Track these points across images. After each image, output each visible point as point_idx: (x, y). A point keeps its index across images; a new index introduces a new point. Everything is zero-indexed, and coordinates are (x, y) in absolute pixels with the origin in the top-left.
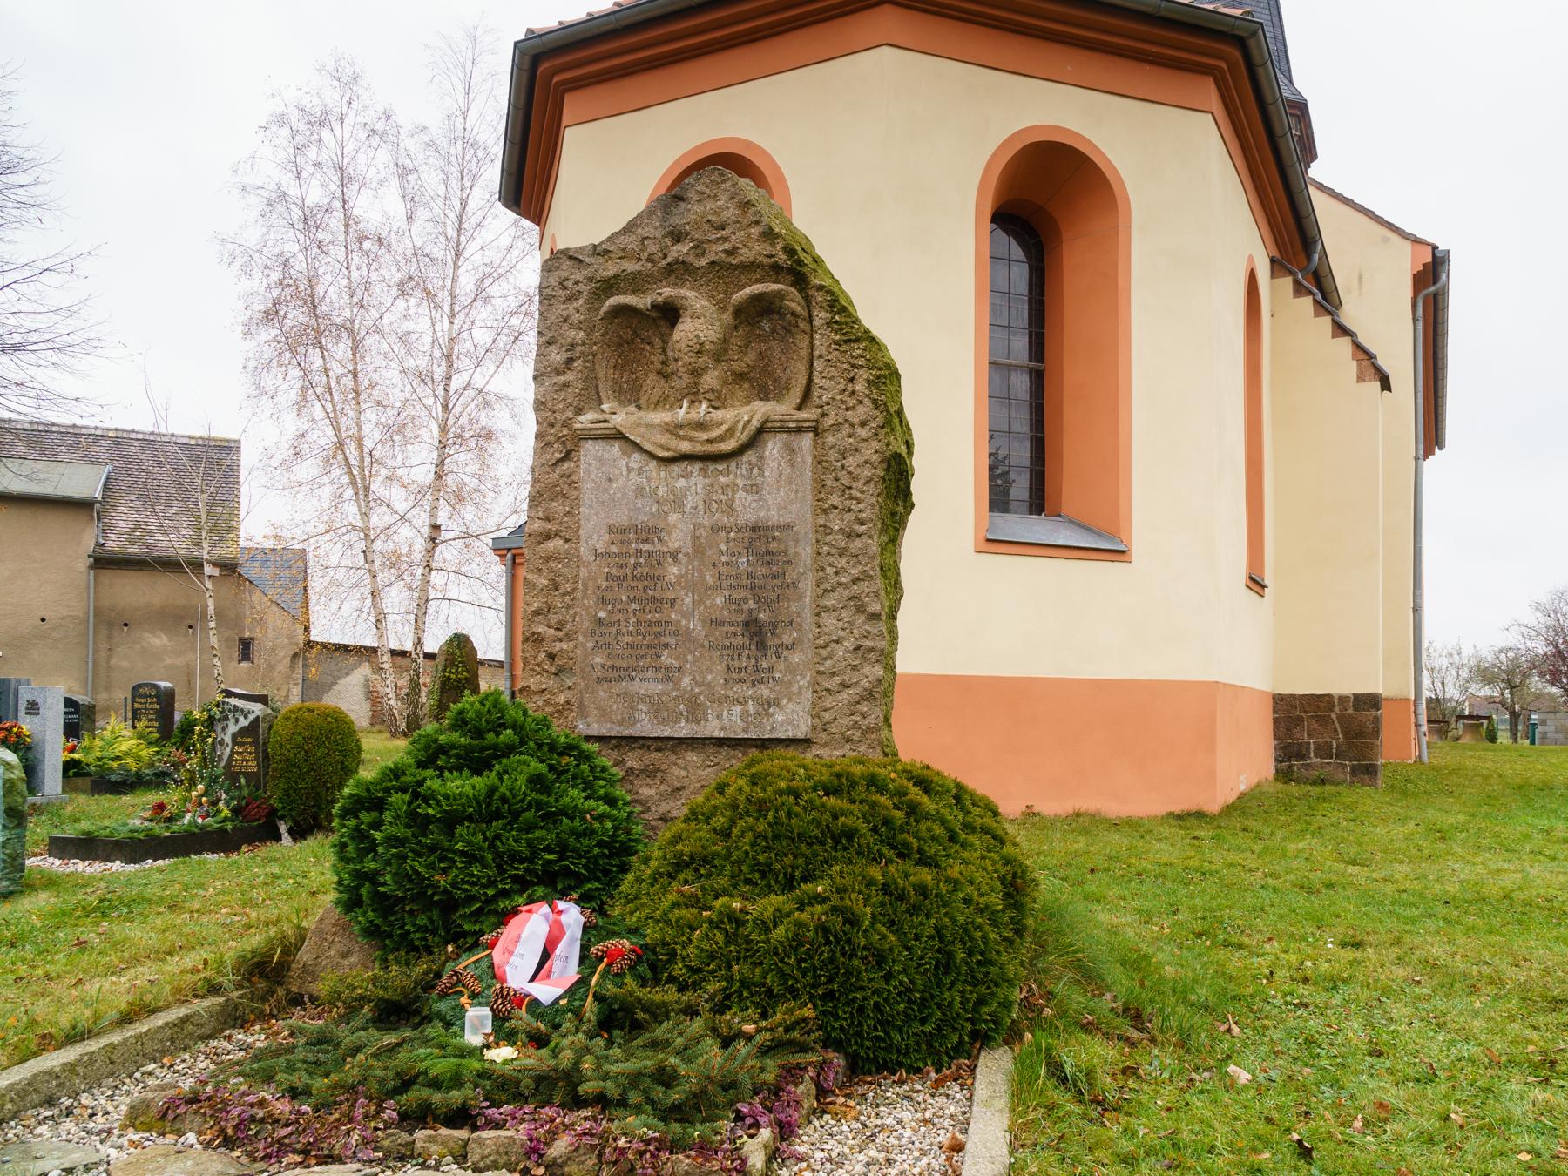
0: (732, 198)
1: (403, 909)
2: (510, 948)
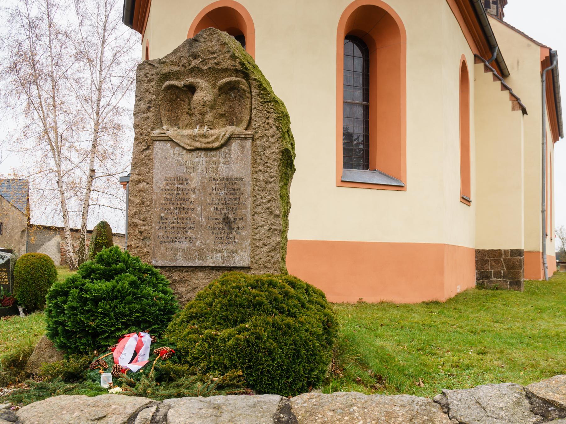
0: (218, 41)
1: (76, 337)
2: (121, 351)
